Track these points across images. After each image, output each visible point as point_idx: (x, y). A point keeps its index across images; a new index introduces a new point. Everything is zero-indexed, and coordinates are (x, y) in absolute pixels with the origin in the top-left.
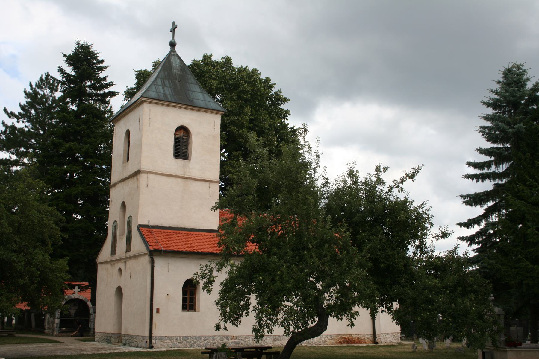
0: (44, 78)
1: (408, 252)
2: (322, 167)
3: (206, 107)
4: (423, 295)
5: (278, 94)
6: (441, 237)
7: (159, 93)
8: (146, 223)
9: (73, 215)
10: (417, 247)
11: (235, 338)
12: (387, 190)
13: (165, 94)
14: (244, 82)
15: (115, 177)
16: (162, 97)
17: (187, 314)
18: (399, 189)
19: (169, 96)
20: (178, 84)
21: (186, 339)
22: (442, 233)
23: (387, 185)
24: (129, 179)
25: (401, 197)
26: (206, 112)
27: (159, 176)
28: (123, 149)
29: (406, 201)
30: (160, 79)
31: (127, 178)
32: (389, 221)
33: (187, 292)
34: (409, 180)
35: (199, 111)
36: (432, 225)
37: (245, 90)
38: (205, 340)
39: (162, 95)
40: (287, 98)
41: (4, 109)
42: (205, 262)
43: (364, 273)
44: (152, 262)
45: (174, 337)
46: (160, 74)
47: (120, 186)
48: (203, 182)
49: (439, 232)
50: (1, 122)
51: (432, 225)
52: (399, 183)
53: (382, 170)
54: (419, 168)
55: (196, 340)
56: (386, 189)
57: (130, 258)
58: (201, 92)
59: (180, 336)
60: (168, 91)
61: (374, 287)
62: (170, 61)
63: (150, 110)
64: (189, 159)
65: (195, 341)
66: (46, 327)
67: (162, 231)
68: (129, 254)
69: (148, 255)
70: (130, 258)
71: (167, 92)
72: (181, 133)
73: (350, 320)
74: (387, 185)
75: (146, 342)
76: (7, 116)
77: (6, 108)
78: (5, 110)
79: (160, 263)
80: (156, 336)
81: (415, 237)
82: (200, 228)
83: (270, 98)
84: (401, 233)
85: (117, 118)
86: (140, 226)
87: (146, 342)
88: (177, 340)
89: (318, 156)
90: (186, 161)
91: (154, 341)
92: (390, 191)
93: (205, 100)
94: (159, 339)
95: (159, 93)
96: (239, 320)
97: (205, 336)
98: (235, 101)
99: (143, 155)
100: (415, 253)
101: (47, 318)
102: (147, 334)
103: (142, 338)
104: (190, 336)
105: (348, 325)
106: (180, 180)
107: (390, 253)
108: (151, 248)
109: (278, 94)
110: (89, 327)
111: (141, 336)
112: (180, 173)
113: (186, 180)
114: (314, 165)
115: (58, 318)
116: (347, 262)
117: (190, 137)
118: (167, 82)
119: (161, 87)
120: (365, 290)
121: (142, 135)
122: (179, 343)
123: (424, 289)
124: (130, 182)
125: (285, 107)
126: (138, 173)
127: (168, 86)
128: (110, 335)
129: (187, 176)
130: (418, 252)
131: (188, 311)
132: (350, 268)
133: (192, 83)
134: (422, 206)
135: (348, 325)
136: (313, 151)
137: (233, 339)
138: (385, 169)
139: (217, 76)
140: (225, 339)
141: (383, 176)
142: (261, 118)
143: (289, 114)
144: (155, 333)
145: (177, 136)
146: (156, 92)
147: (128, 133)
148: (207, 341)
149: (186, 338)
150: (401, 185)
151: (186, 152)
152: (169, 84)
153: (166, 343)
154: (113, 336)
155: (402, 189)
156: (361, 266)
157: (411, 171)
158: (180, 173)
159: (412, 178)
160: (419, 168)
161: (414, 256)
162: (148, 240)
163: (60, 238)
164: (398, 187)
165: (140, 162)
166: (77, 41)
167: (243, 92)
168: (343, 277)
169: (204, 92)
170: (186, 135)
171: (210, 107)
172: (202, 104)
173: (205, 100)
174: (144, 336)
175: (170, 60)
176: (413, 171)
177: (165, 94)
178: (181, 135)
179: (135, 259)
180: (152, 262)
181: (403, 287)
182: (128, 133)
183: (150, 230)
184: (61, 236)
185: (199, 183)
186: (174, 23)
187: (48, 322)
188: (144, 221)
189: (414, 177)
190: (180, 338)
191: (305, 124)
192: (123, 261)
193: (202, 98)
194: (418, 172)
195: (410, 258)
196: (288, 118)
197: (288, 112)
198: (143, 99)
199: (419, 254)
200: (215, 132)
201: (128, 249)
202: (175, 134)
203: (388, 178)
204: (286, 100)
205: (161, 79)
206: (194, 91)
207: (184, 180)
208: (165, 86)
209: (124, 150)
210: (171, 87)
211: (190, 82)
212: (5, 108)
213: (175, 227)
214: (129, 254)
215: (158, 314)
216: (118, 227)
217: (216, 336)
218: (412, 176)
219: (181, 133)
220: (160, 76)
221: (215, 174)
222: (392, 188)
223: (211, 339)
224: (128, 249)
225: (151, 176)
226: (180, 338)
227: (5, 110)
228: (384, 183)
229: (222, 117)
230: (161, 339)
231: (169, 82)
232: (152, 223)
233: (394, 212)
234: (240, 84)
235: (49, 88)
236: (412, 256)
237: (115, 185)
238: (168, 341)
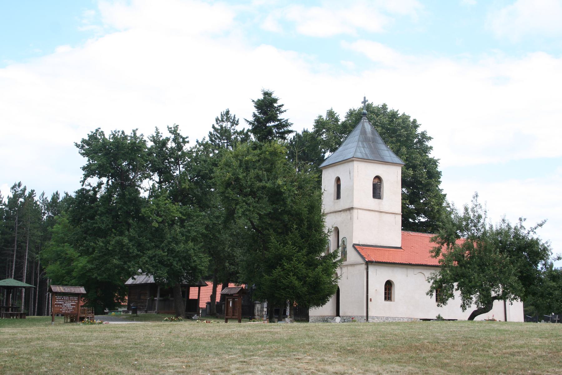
5: (423, 134)
6: (557, 259)
8: (357, 243)
10: (544, 265)
16: (365, 157)
17: (388, 303)
20: (372, 145)
22: (558, 257)
25: (535, 237)
26: (392, 165)
28: (333, 190)
29: (537, 239)
31: (340, 211)
35: (388, 165)
42: (433, 271)
43: (517, 279)
44: (367, 269)
48: (391, 214)
49: (556, 257)
51: (552, 254)
52: (533, 229)
53: (523, 220)
56: (526, 232)
62: (364, 127)
66: (256, 314)
69: (364, 264)
71: (367, 153)
79: (371, 269)
83: (417, 136)
88: (382, 319)
94: (372, 318)
100: (542, 268)
101: (257, 308)
102: (365, 314)
106: (377, 213)
109: (423, 134)
114: (483, 216)
115: (266, 308)
118: (365, 144)
119: (362, 149)
123: (548, 288)
124: (343, 215)
125: (428, 144)
127: (367, 147)
129: (382, 211)
133: (380, 143)
134: (547, 243)
138: (525, 219)
139: (380, 123)
141: (524, 224)
143: (432, 150)
144: (370, 314)
149: (387, 318)
150: (535, 230)
152: (367, 145)
155: (535, 232)
156: (515, 275)
157: (540, 222)
162: (363, 255)
164: (533, 231)
165: (352, 201)
167: (400, 136)
168: (506, 280)
171: (395, 162)
172: (388, 159)
173: (391, 157)
180: (367, 269)
181: (536, 286)
183: (362, 247)
186: (365, 98)
187: (258, 310)
193: (389, 155)
203: (528, 225)
204: (430, 138)
205: (361, 142)
208: (364, 147)
209: (334, 191)
211: (379, 142)
221: (399, 210)
225: (359, 211)
230: (373, 318)
232: (361, 243)
233: (531, 245)
234: (397, 129)
236: (540, 270)
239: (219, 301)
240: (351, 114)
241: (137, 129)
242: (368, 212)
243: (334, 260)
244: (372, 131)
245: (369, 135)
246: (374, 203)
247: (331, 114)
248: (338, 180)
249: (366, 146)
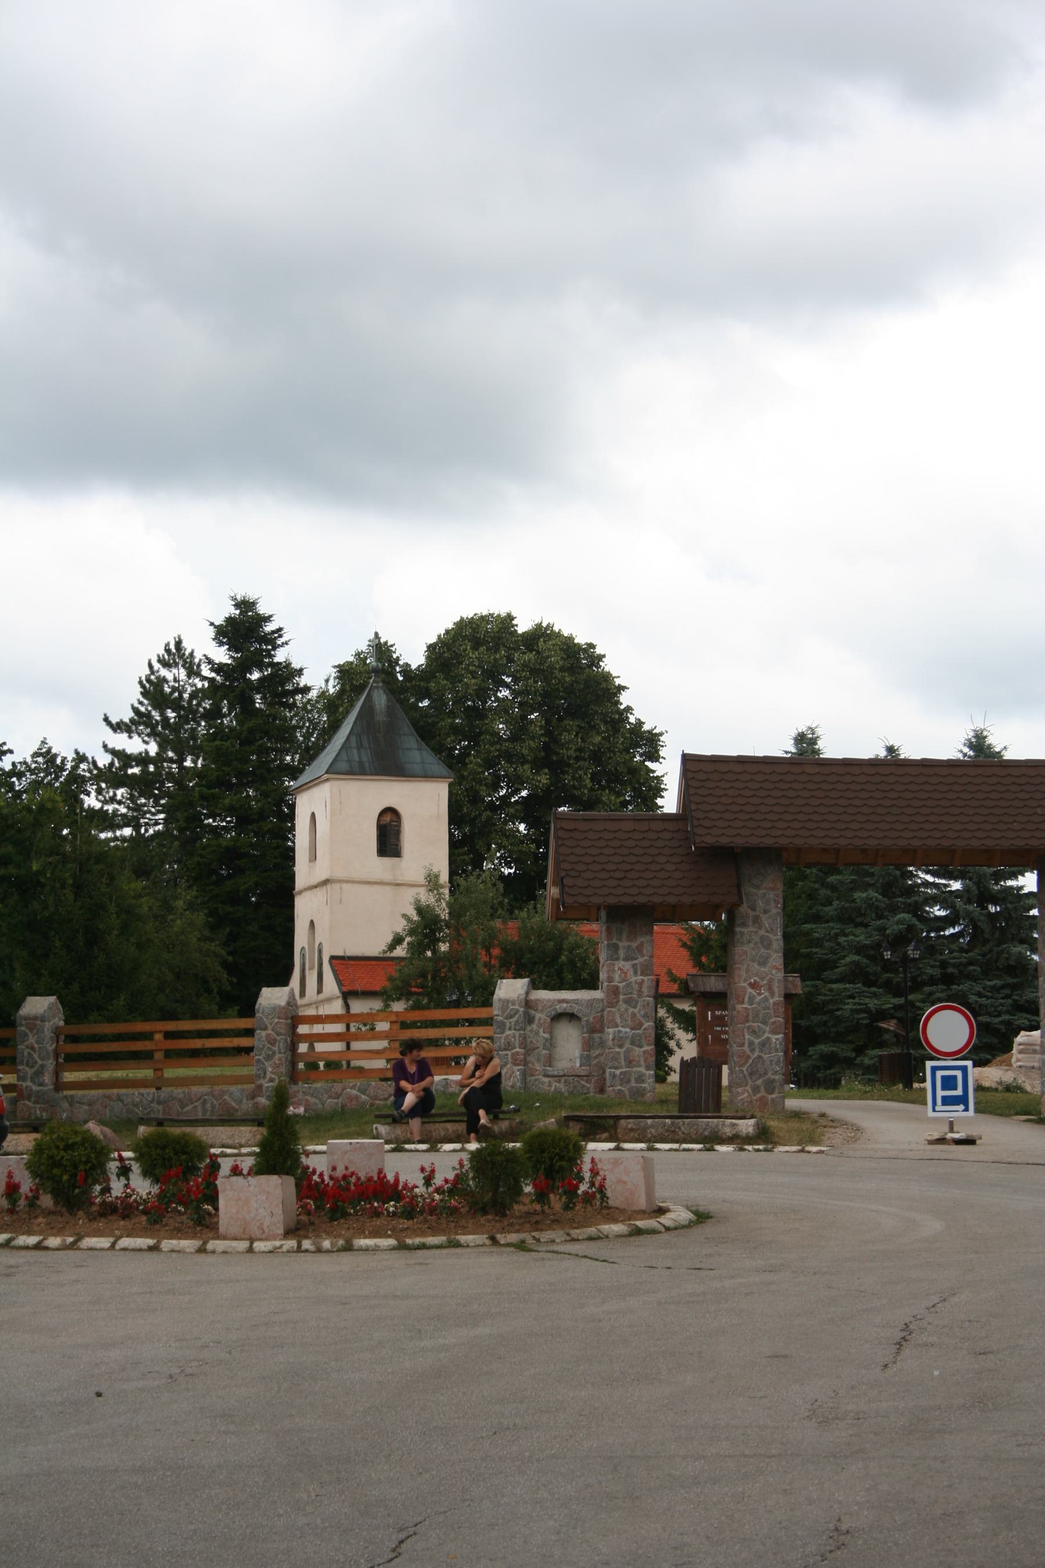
0: (172, 647)
8: (340, 953)
9: (258, 696)
13: (361, 763)
15: (300, 882)
19: (367, 765)
27: (356, 885)
31: (315, 887)
41: (103, 717)
46: (344, 757)
47: (307, 895)
50: (102, 745)
57: (323, 1001)
58: (418, 749)
60: (366, 757)
67: (358, 963)
68: (322, 996)
70: (323, 1001)
71: (364, 759)
72: (387, 818)
76: (110, 731)
77: (108, 715)
78: (106, 719)
86: (333, 958)
90: (396, 859)
106: (387, 888)
108: (345, 989)
119: (355, 751)
127: (367, 746)
145: (382, 823)
151: (397, 845)
158: (387, 877)
163: (228, 983)
166: (233, 595)
173: (423, 763)
177: (361, 763)
183: (345, 962)
184: (228, 980)
192: (314, 1006)
193: (418, 760)
201: (320, 991)
202: (378, 820)
206: (407, 749)
207: (393, 887)
212: (105, 715)
214: (322, 996)
216: (307, 956)
220: (355, 731)
224: (320, 991)
225: (345, 886)
227: (106, 719)
229: (450, 785)
232: (349, 953)
235: (183, 666)
237: (300, 892)
239: (166, 1075)
240: (345, 672)
241: (212, 624)
242: (366, 887)
243: (997, 884)
244: (388, 707)
245: (381, 717)
246: (381, 867)
247: (382, 650)
248: (313, 815)
249: (365, 743)
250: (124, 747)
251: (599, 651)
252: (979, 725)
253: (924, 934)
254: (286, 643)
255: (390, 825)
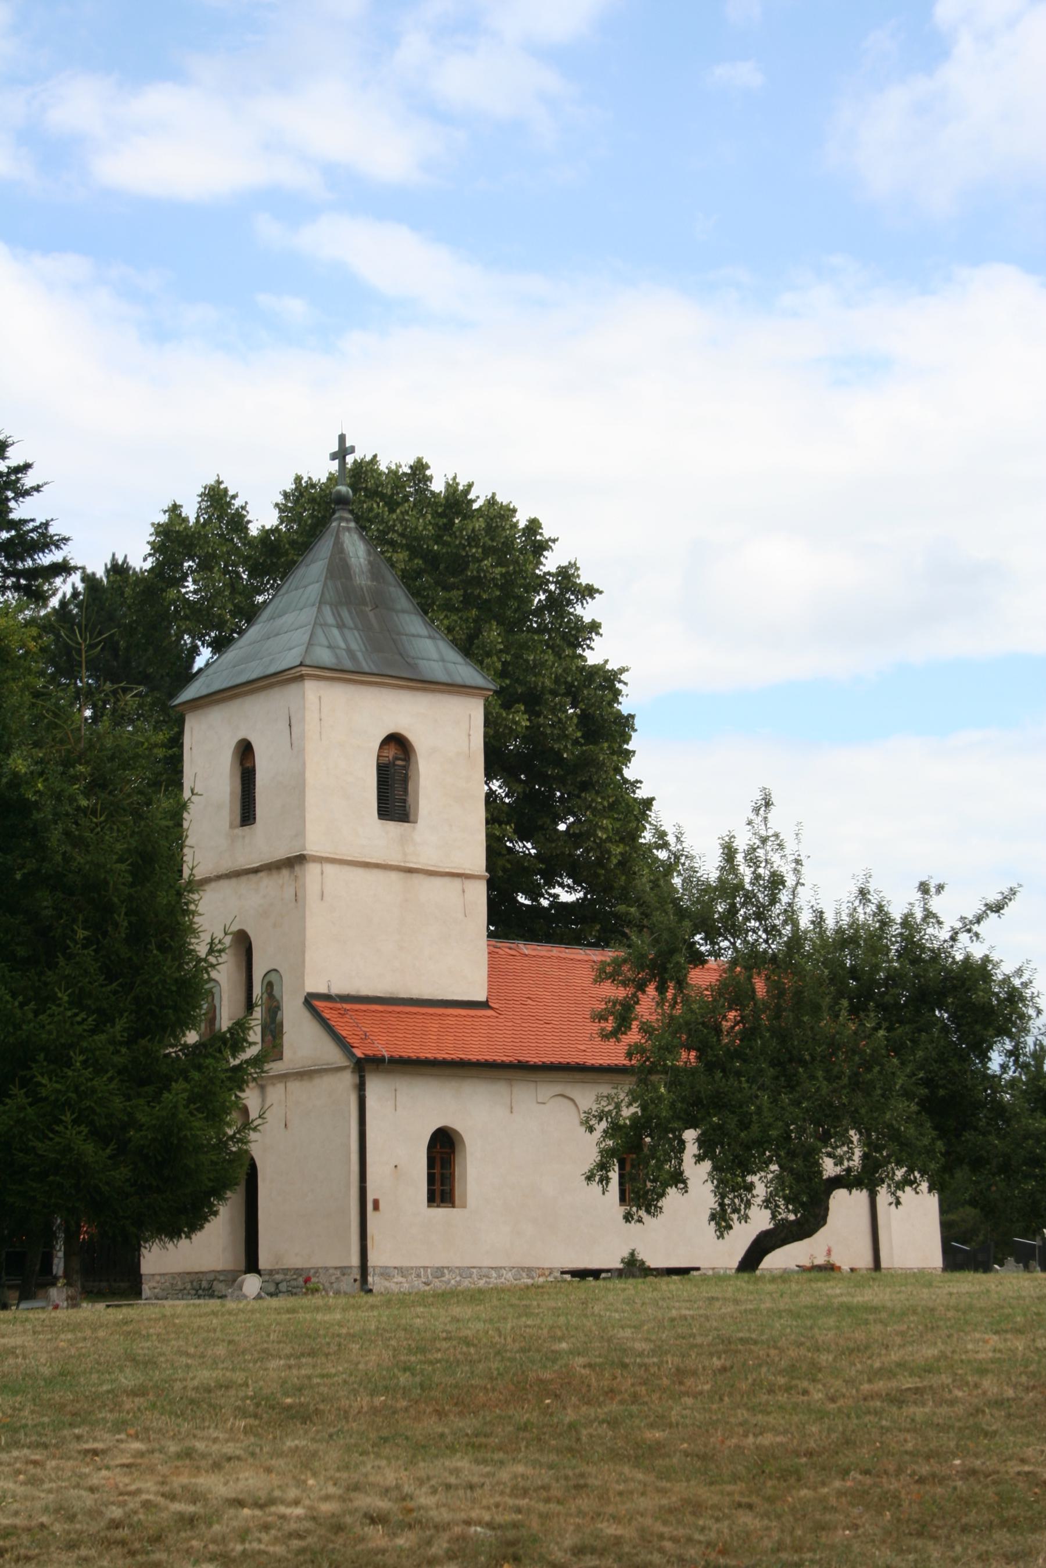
1: (990, 1065)
2: (808, 885)
3: (449, 681)
4: (1023, 1148)
7: (338, 651)
8: (322, 989)
11: (547, 1273)
12: (947, 938)
14: (480, 550)
16: (348, 664)
17: (441, 1213)
18: (971, 934)
20: (371, 615)
21: (439, 1274)
23: (947, 927)
24: (261, 874)
25: (977, 952)
26: (449, 692)
29: (986, 959)
30: (328, 607)
31: (256, 871)
32: (953, 1003)
33: (434, 1158)
34: (993, 916)
35: (433, 691)
36: (1039, 1012)
37: (485, 576)
38: (480, 1278)
39: (344, 653)
40: (595, 587)
42: (605, 1090)
43: (914, 1108)
45: (412, 1268)
53: (933, 890)
54: (1013, 892)
55: (461, 1276)
56: (945, 934)
58: (430, 637)
59: (425, 1268)
61: (934, 1133)
63: (320, 698)
64: (412, 818)
65: (458, 1279)
67: (390, 1008)
71: (354, 646)
73: (893, 1194)
74: (947, 927)
75: (355, 1280)
79: (377, 1088)
80: (374, 1267)
81: (1003, 1031)
82: (445, 998)
83: (541, 582)
84: (978, 1027)
85: (202, 702)
87: (355, 1280)
88: (418, 1276)
89: (798, 862)
91: (370, 1279)
92: (953, 939)
93: (443, 660)
94: (382, 1274)
95: (338, 651)
96: (659, 1204)
97: (480, 1268)
98: (458, 610)
99: (309, 817)
100: (1004, 1067)
102: (355, 1261)
103: (338, 1272)
104: (448, 1268)
105: (891, 1204)
106: (394, 876)
107: (957, 1068)
108: (358, 1053)
110: (54, 1272)
111: (336, 1268)
112: (395, 860)
113: (408, 875)
114: (790, 880)
116: (881, 1088)
117: (412, 760)
118: (345, 614)
119: (335, 632)
120: (917, 1139)
121: (304, 764)
122: (425, 1283)
123: (1026, 1138)
124: (268, 884)
125: (586, 611)
126: (295, 862)
127: (352, 625)
128: (211, 1277)
130: (1011, 1064)
131: (438, 1206)
132: (887, 1099)
133: (403, 611)
134: (1019, 972)
135: (891, 1204)
136: (787, 851)
137: (543, 1275)
138: (940, 888)
140: (524, 1274)
141: (936, 904)
142: (532, 657)
143: (597, 634)
144: (373, 1260)
146: (330, 647)
147: (245, 751)
148: (485, 1279)
149: (439, 1272)
150: (975, 928)
151: (405, 801)
153: (397, 1283)
154: (222, 1278)
155: (977, 935)
156: (908, 1095)
157: (993, 897)
159: (997, 911)
160: (1013, 892)
161: (1003, 1073)
162: (344, 1033)
164: (969, 931)
165: (300, 833)
168: (876, 1115)
169: (436, 635)
170: (402, 756)
172: (435, 670)
173: (443, 660)
174: (345, 1267)
175: (342, 545)
176: (999, 897)
178: (391, 758)
179: (301, 1080)
182: (245, 751)
183: (339, 1006)
185: (438, 882)
186: (342, 438)
188: (315, 985)
189: (1002, 908)
190: (426, 1272)
191: (765, 789)
193: (435, 655)
194: (1010, 900)
195: (994, 1076)
196: (593, 645)
197: (594, 627)
198: (305, 671)
199: (1013, 1068)
200: (472, 745)
205: (331, 605)
206: (413, 636)
207: (402, 875)
210: (356, 628)
211: (399, 607)
213: (388, 996)
215: (377, 1213)
217: (504, 1268)
218: (997, 908)
219: (391, 752)
220: (327, 596)
221: (476, 859)
222: (957, 933)
223: (494, 1275)
225: (329, 868)
226: (426, 1272)
228: (939, 923)
230: (386, 1273)
231: (350, 613)
232: (335, 990)
238: (400, 1279)
242: (360, 872)
244: (370, 562)
245: (362, 580)
250: (95, 570)
251: (280, 499)
252: (241, 735)
253: (896, 964)
254: (37, 489)
255: (395, 765)
